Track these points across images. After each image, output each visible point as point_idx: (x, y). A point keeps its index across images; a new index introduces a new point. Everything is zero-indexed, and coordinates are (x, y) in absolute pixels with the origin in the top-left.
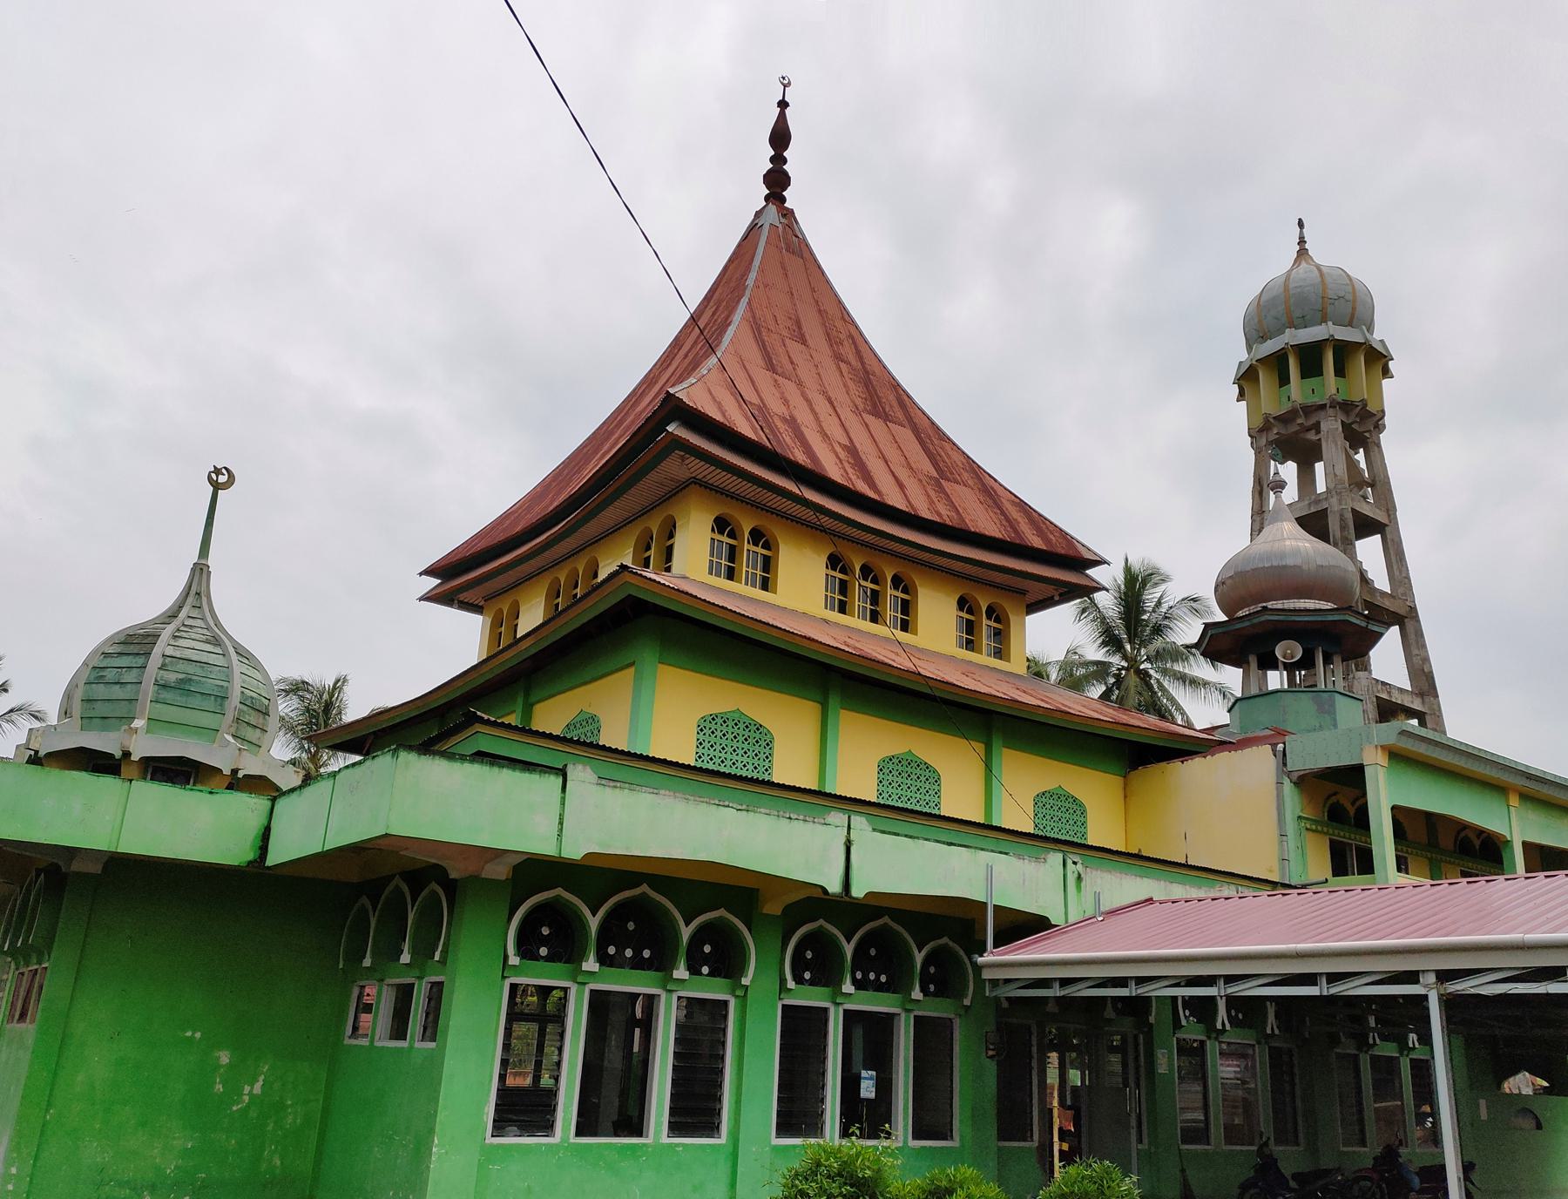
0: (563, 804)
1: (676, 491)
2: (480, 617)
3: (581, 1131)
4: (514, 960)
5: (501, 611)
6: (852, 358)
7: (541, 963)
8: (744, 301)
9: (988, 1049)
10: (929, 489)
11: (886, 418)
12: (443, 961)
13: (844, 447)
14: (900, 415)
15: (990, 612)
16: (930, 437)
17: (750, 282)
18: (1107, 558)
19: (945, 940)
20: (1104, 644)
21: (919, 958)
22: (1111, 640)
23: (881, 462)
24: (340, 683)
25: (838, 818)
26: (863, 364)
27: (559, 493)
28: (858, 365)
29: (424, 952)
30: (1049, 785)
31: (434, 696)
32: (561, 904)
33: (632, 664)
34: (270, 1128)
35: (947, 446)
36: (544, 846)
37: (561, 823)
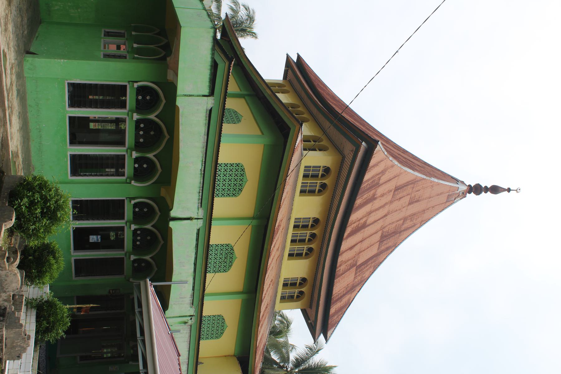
0: (198, 96)
1: (339, 150)
2: (282, 79)
3: (71, 118)
4: (136, 85)
5: (285, 86)
6: (405, 226)
7: (135, 97)
8: (424, 177)
9: (113, 290)
10: (352, 261)
11: (381, 241)
12: (134, 58)
13: (365, 222)
14: (383, 248)
15: (301, 293)
16: (374, 262)
17: (433, 179)
18: (329, 342)
19: (156, 269)
20: (297, 359)
21: (147, 258)
22: (298, 363)
23: (360, 239)
24: (254, 35)
25: (201, 213)
26: (404, 230)
27: (335, 105)
28: (402, 229)
29: (138, 51)
30: (227, 322)
31: (245, 59)
32: (159, 100)
33: (263, 134)
34: (69, 4)
35: (371, 270)
36: (179, 92)
37: (190, 96)
